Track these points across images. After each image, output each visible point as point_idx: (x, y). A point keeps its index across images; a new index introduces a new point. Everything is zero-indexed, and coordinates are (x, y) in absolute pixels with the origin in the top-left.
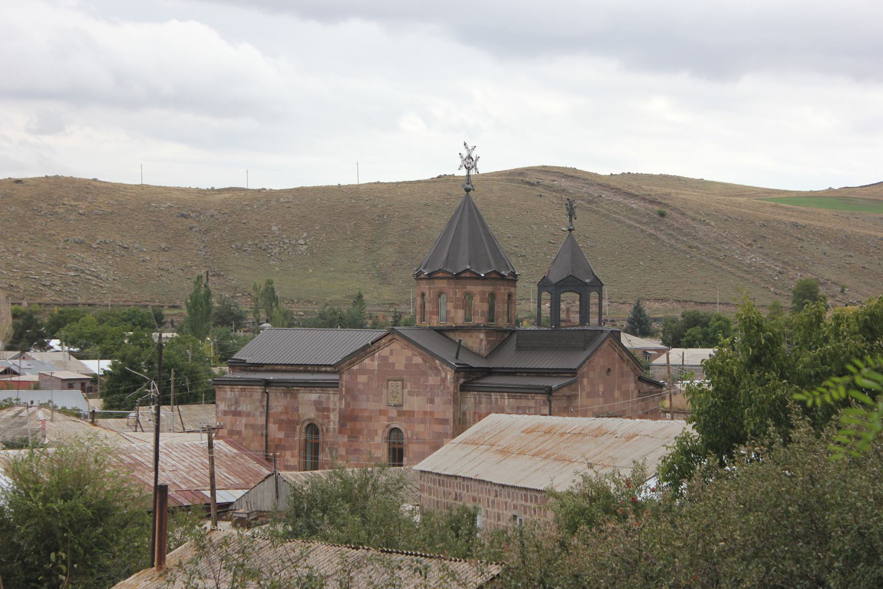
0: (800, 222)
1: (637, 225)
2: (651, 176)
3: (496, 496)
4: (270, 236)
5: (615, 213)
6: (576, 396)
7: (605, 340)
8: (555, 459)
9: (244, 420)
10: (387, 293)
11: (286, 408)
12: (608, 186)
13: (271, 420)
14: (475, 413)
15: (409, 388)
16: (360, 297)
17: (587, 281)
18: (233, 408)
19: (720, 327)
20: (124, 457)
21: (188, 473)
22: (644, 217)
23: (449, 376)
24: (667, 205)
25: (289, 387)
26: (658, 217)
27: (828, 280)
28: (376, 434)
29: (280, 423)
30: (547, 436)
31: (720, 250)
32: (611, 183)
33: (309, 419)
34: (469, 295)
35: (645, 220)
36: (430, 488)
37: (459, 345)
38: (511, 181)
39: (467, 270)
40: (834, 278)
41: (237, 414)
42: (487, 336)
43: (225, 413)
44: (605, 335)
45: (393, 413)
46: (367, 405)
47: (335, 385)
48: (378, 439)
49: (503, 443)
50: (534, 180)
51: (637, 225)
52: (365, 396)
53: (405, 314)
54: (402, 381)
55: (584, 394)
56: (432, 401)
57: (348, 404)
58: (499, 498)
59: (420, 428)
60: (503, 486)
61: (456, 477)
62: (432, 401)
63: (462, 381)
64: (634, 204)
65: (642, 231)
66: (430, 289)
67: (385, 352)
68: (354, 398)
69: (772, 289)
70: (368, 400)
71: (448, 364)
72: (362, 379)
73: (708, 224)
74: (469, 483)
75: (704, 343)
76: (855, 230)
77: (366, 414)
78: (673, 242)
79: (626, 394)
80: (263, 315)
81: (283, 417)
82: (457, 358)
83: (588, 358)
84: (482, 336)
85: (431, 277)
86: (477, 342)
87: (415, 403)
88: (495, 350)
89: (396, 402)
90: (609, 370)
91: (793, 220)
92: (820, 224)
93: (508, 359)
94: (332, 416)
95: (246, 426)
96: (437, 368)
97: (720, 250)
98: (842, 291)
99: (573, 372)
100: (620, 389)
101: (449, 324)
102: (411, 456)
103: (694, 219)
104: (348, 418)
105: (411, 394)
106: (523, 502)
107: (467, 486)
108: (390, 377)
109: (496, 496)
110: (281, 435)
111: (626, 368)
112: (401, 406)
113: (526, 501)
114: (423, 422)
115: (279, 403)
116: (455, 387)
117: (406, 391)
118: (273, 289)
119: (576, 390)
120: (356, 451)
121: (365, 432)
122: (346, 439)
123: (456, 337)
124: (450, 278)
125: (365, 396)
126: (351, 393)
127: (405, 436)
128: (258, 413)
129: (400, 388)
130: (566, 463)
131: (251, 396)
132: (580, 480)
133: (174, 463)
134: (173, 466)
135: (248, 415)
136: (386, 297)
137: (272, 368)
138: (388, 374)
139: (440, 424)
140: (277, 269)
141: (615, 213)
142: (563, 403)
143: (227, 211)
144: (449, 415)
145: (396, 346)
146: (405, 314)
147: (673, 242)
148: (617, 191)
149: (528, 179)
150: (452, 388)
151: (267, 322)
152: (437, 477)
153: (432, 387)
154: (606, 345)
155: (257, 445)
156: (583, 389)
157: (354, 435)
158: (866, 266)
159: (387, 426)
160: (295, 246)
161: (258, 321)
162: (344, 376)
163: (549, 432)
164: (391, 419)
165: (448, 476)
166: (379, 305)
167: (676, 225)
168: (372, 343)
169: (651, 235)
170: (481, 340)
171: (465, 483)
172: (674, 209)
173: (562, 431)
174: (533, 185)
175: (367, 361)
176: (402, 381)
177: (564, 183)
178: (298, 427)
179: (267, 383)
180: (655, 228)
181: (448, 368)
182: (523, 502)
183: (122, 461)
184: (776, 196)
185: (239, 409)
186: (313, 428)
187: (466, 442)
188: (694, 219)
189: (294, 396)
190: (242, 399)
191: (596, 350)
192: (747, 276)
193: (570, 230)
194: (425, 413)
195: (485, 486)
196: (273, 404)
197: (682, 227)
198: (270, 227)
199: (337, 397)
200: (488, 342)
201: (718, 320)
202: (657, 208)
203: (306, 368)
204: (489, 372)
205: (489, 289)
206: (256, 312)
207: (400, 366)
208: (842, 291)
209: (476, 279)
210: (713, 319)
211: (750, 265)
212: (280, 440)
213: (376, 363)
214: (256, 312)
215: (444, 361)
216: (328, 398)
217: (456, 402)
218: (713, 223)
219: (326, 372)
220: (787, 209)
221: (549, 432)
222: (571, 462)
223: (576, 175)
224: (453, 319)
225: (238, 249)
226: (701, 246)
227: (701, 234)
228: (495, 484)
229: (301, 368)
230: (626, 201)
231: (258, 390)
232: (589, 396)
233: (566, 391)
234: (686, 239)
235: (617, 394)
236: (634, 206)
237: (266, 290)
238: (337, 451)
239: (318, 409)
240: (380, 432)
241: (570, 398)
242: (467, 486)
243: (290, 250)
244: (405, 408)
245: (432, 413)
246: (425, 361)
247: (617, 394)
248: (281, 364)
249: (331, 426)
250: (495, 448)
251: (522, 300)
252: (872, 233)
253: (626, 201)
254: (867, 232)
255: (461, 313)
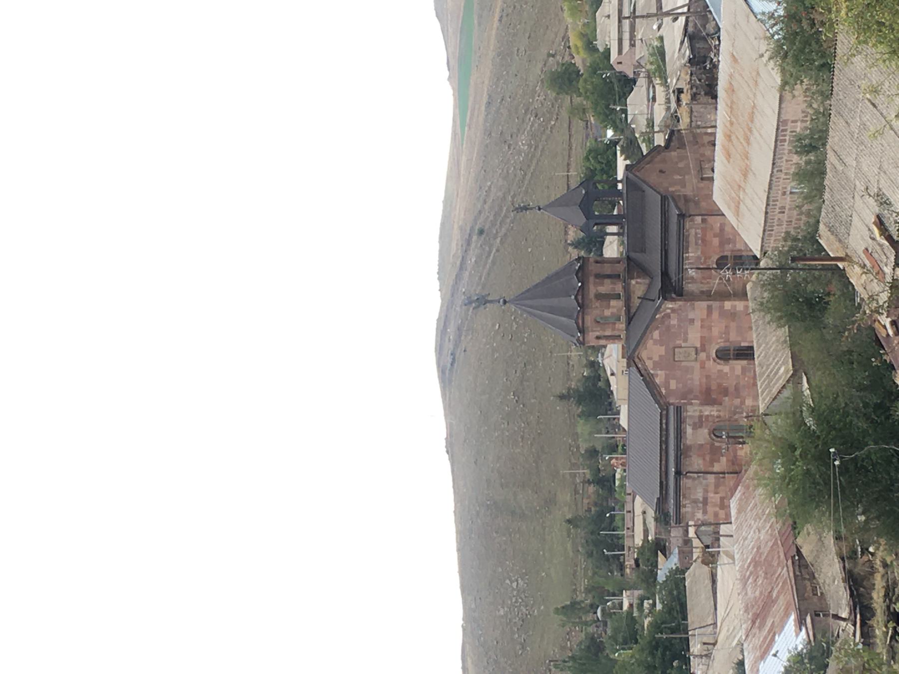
0: (485, 99)
1: (491, 257)
2: (440, 251)
3: (781, 171)
4: (509, 616)
5: (480, 278)
6: (685, 196)
7: (636, 176)
8: (752, 121)
9: (711, 495)
10: (565, 497)
11: (699, 456)
12: (453, 286)
13: (710, 469)
14: (702, 283)
15: (681, 342)
16: (569, 521)
17: (584, 192)
18: (701, 505)
19: (595, 158)
20: (748, 573)
21: (760, 519)
22: (484, 249)
23: (670, 305)
24: (472, 229)
25: (682, 453)
26: (484, 236)
27: (542, 71)
28: (720, 371)
29: (712, 462)
30: (733, 137)
31: (515, 175)
32: (451, 283)
33: (709, 434)
34: (600, 297)
35: (487, 249)
36: (775, 240)
37: (643, 298)
38: (450, 381)
39: (576, 298)
40: (540, 65)
41: (705, 501)
42: (633, 278)
43: (705, 512)
44: (631, 175)
45: (703, 355)
46: (696, 379)
47: (679, 410)
48: (726, 369)
49: (738, 177)
50: (450, 360)
51: (491, 257)
52: (689, 382)
53: (585, 477)
54: (674, 348)
55: (683, 190)
56: (692, 321)
57: (696, 398)
58: (783, 168)
59: (715, 331)
60: (774, 164)
61: (766, 213)
62: (692, 321)
63: (674, 295)
64: (471, 260)
65: (498, 251)
66: (593, 331)
67: (649, 364)
68: (690, 391)
69: (553, 123)
70: (692, 379)
71: (660, 306)
72: (673, 385)
73: (490, 187)
74: (771, 199)
75: (611, 173)
76: (492, 48)
77: (704, 380)
78: (508, 220)
79: (682, 158)
80: (590, 617)
81: (708, 458)
82: (654, 301)
83: (651, 188)
84: (633, 282)
85: (582, 331)
86: (639, 286)
87: (694, 336)
88: (644, 271)
89: (693, 353)
90: (661, 171)
91: (483, 108)
92: (486, 82)
93: (654, 260)
94: (706, 413)
95: (716, 493)
96: (663, 317)
97: (515, 175)
98: (553, 56)
99: (664, 199)
100: (677, 163)
101: (623, 313)
102: (739, 339)
103: (485, 202)
104: (709, 397)
105: (686, 340)
106: (786, 144)
107: (774, 201)
108: (672, 359)
109: (781, 171)
110: (724, 460)
111: (659, 158)
112: (696, 349)
113: (785, 141)
114: (710, 328)
115: (696, 462)
116: (680, 300)
117: (683, 345)
118: (563, 607)
119: (679, 196)
120: (737, 389)
121: (718, 381)
122: (727, 399)
123: (636, 302)
124: (583, 313)
125: (689, 382)
126: (686, 394)
127: (722, 345)
128: (704, 482)
129: (681, 350)
130: (755, 111)
131: (689, 488)
132: (772, 62)
133: (752, 532)
134: (754, 532)
135: (706, 491)
136: (568, 498)
137: (664, 474)
138: (670, 362)
139: (711, 313)
140: (542, 607)
141: (480, 278)
142: (692, 205)
143: (485, 659)
144: (704, 304)
145: (644, 355)
146: (585, 477)
147: (508, 220)
148: (458, 278)
149: (449, 365)
150: (680, 303)
151: (596, 613)
152: (767, 233)
153: (680, 320)
154: (638, 174)
155: (730, 480)
156: (679, 191)
157: (725, 392)
158: (527, 35)
159: (714, 361)
160: (518, 591)
161: (595, 622)
162: (671, 401)
163: (730, 136)
164: (708, 358)
165: (765, 221)
166: (576, 505)
167: (491, 218)
168: (642, 375)
169: (502, 242)
170: (637, 283)
171: (771, 203)
172: (475, 220)
173: (728, 124)
174: (454, 359)
175: (657, 381)
176: (674, 348)
177: (451, 330)
178: (717, 444)
179: (678, 473)
180: (495, 238)
181: (663, 306)
182: (786, 144)
183: (751, 573)
184: (459, 131)
185: (701, 499)
186: (715, 433)
187: (737, 213)
188: (485, 202)
189: (689, 448)
190: (692, 497)
191: (644, 182)
192: (540, 147)
193: (540, 209)
194: (702, 327)
195: (774, 183)
196: (695, 468)
197: (493, 213)
198: (502, 616)
199: (689, 407)
200: (638, 277)
201: (589, 160)
202: (475, 238)
203: (664, 442)
204: (665, 274)
205: (592, 279)
206: (586, 623)
207: (662, 350)
208: (553, 56)
209: (583, 289)
210: (588, 164)
211: (530, 146)
212: (728, 461)
213: (659, 372)
214: (586, 623)
215: (658, 310)
216: (691, 417)
217: (693, 298)
218: (489, 183)
219: (667, 424)
220: (472, 115)
221: (728, 137)
222: (754, 107)
223: (443, 319)
224: (619, 310)
225: (523, 648)
226: (512, 193)
227: (500, 194)
228: (772, 172)
229: (664, 447)
230: (469, 269)
231: (685, 482)
232: (684, 186)
233: (681, 204)
234: (505, 208)
235: (681, 165)
236: (473, 260)
237: (565, 614)
238: (736, 407)
239: (701, 427)
240: (719, 367)
241: (687, 199)
242: (774, 201)
243: (523, 596)
244: (698, 345)
245: (702, 320)
246: (657, 328)
247: (681, 165)
248: (661, 464)
249: (715, 413)
250: (742, 184)
251: (568, 364)
252: (494, 32)
253: (469, 269)
254: (493, 37)
255: (613, 303)
